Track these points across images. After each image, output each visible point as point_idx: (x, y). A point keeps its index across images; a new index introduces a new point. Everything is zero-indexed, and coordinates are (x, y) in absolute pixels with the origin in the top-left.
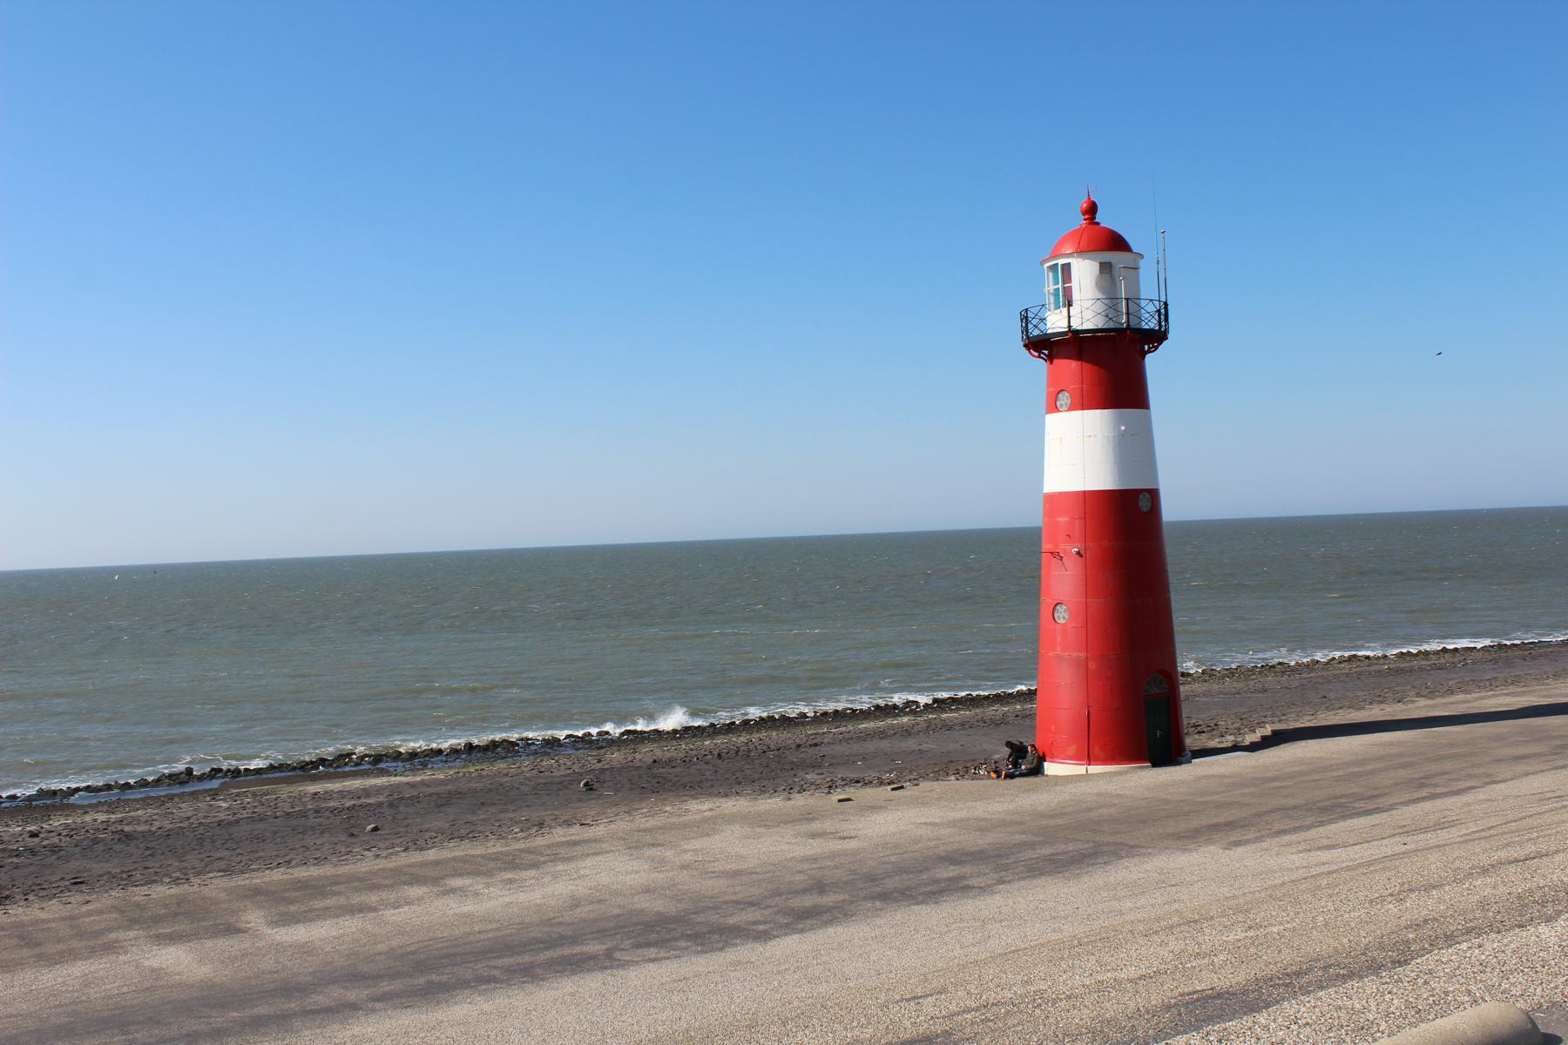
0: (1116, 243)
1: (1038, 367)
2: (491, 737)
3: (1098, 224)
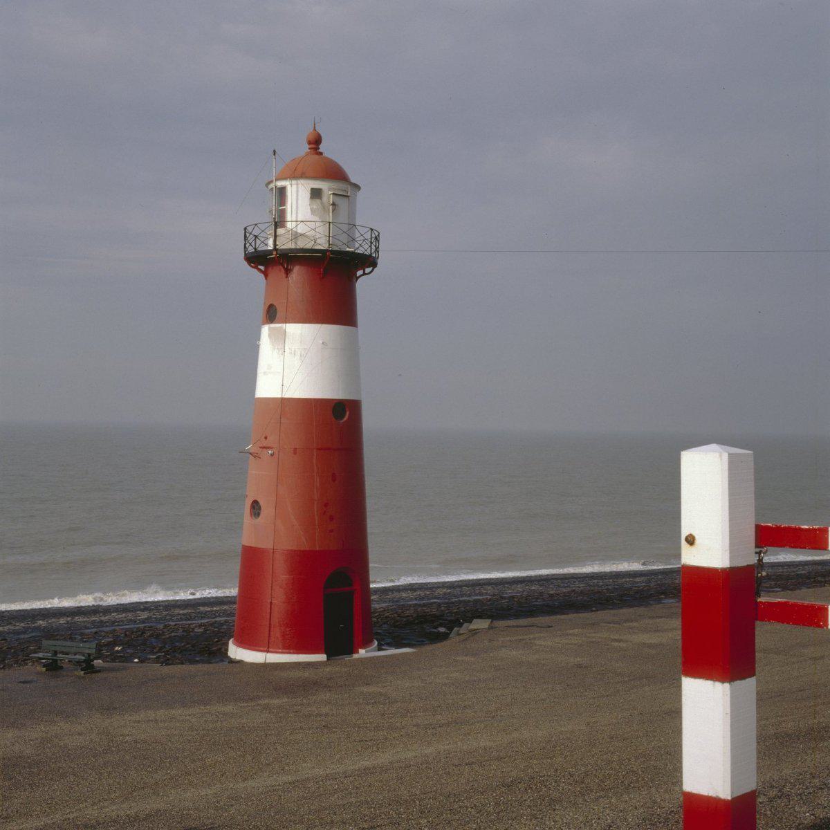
0: (334, 173)
1: (255, 277)
2: (795, 601)
3: (321, 154)
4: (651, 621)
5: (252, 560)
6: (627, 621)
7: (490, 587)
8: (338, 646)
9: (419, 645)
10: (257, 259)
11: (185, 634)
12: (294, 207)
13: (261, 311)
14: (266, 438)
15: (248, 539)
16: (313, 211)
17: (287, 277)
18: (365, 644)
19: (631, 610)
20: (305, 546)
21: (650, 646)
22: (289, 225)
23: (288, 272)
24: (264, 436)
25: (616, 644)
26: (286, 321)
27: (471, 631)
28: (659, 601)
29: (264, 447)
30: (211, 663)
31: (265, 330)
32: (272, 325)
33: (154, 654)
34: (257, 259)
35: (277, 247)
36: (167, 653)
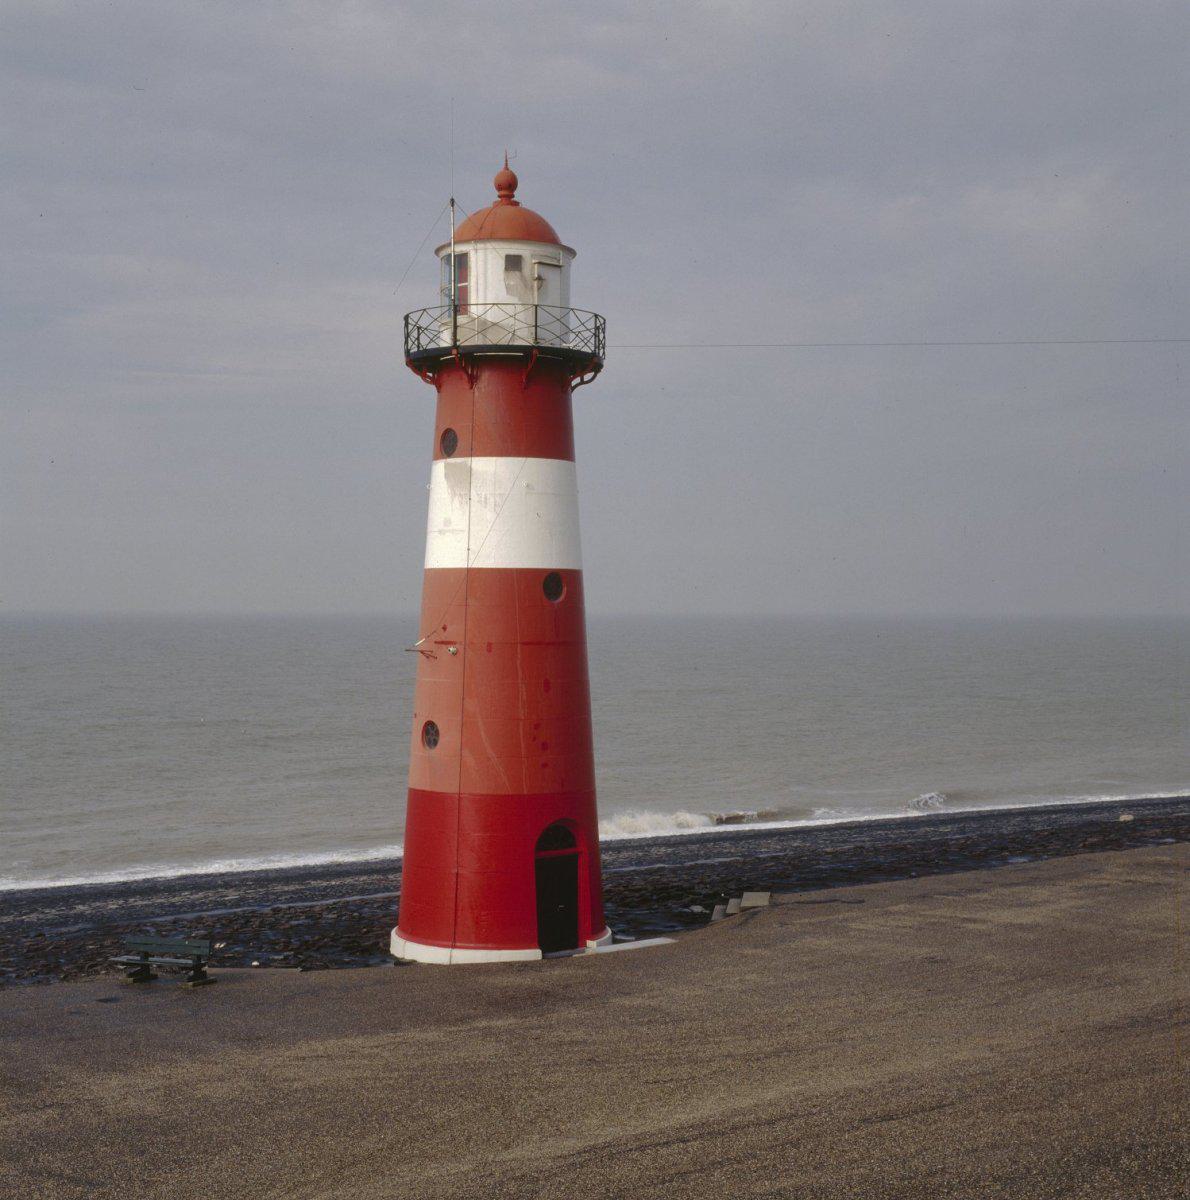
0: (537, 231)
3: (516, 204)
4: (1006, 891)
5: (426, 811)
6: (970, 891)
7: (727, 844)
8: (560, 936)
9: (670, 932)
10: (427, 363)
11: (311, 922)
12: (481, 281)
13: (430, 437)
14: (445, 628)
15: (418, 780)
16: (508, 289)
17: (472, 388)
18: (595, 932)
19: (969, 875)
20: (506, 788)
21: (1022, 927)
22: (473, 310)
23: (473, 380)
24: (442, 625)
25: (971, 926)
26: (472, 453)
27: (744, 910)
28: (1004, 861)
29: (443, 643)
30: (367, 966)
31: (439, 467)
32: (451, 460)
33: (278, 953)
34: (427, 363)
35: (458, 343)
36: (298, 951)
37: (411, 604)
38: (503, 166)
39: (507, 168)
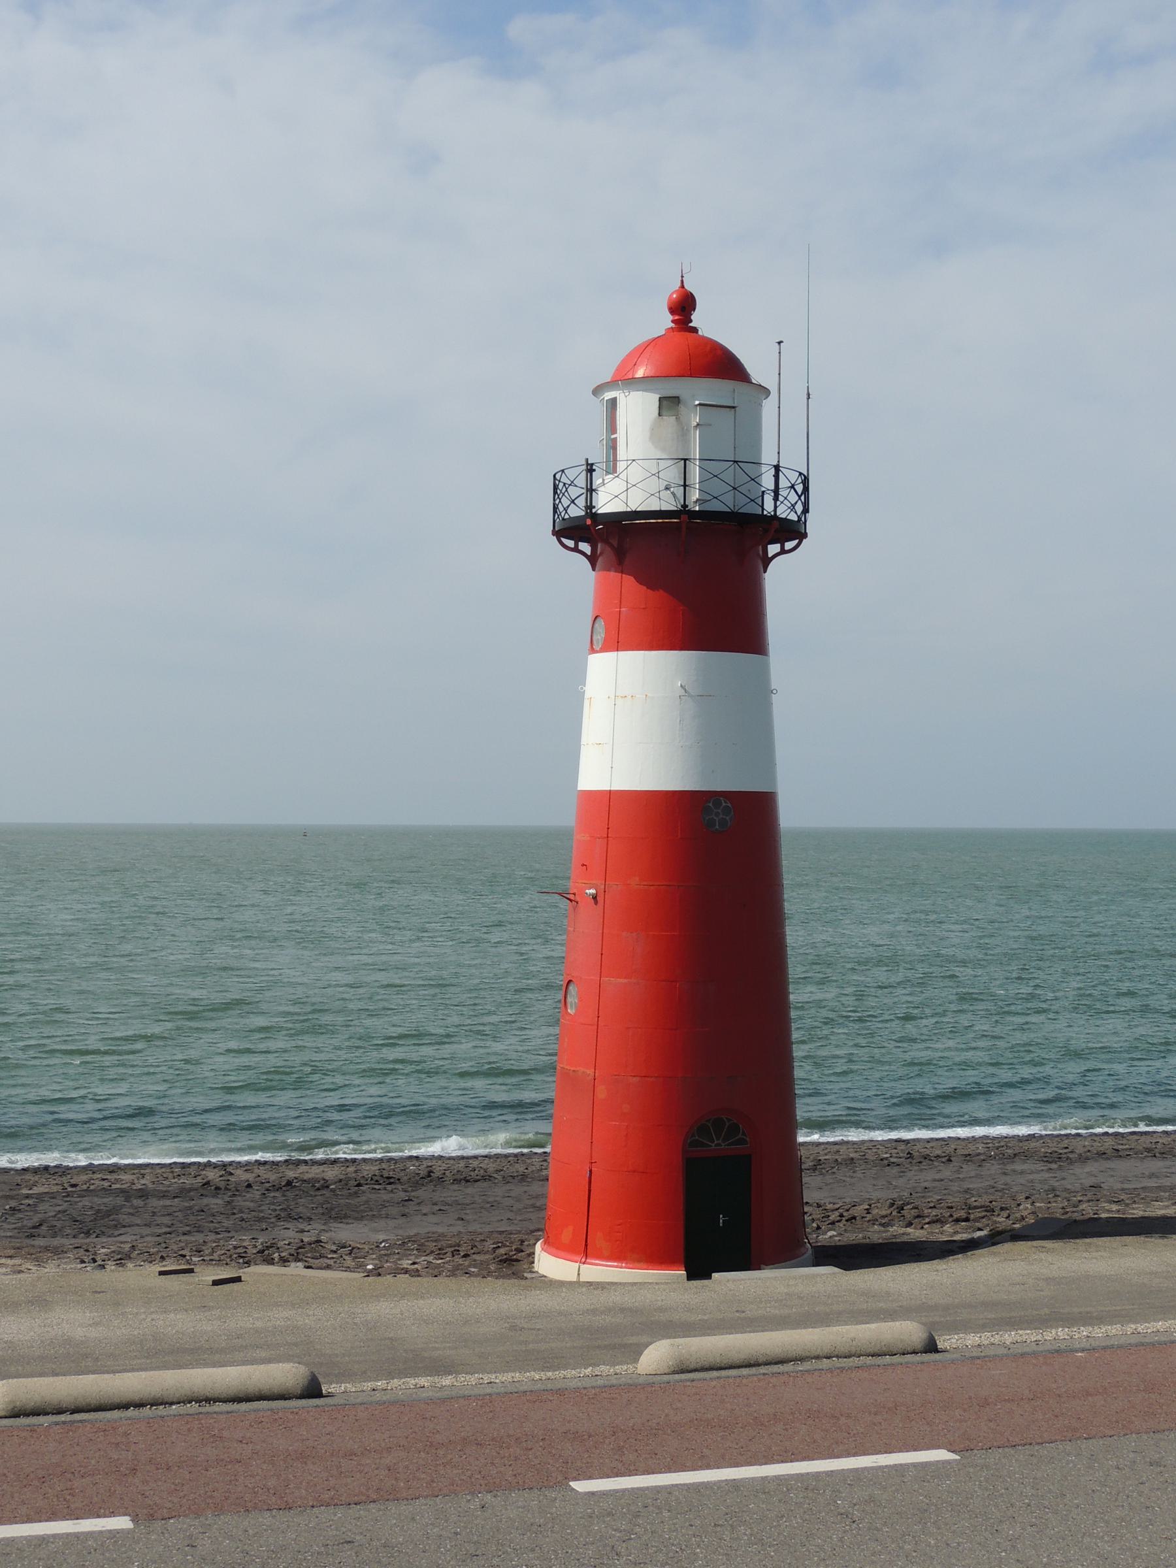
37: (567, 817)
38: (679, 284)
39: (683, 286)
